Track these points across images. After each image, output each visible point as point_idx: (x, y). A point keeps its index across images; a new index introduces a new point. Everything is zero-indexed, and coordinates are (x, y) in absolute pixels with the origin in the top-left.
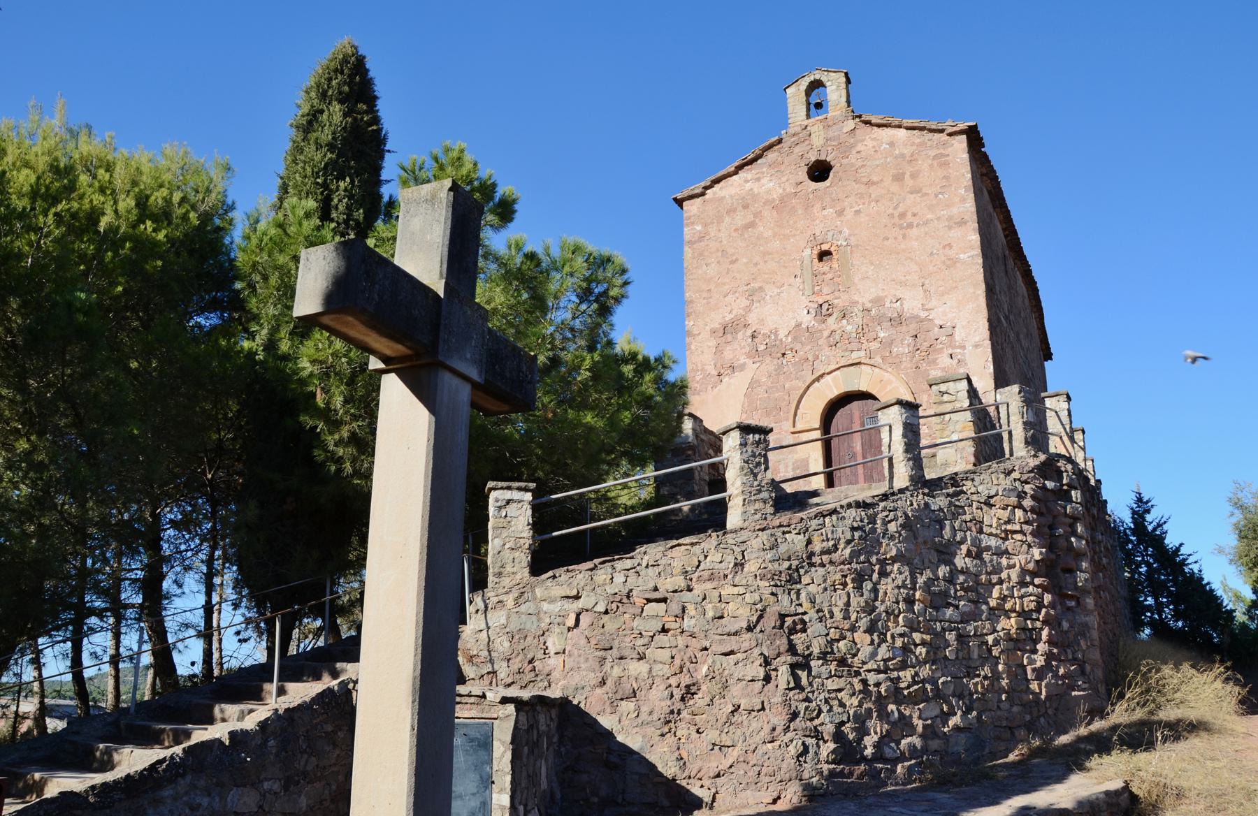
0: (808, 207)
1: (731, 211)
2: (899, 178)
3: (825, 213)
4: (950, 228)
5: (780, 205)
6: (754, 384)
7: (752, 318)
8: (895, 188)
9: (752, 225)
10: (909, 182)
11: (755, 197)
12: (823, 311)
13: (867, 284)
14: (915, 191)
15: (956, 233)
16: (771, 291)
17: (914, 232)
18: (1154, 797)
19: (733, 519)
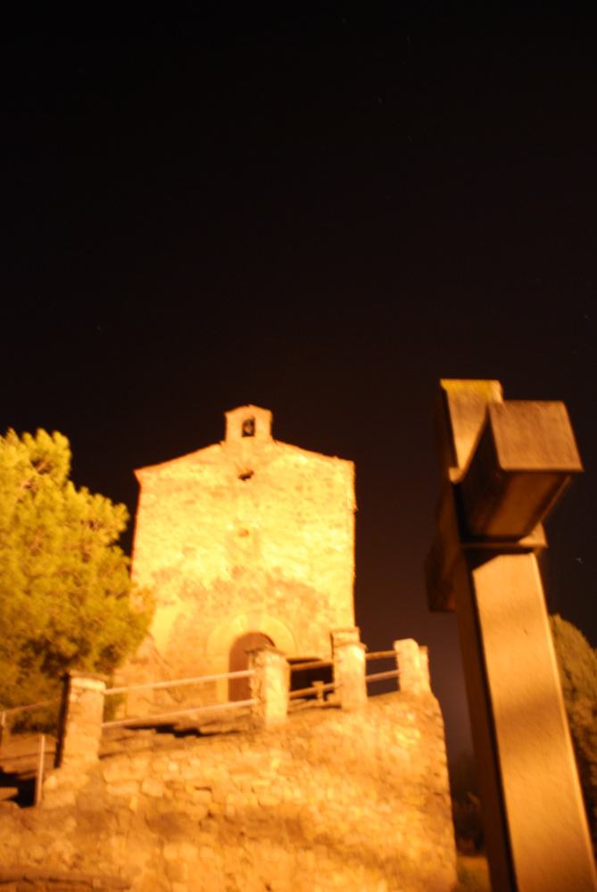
0: (235, 496)
1: (179, 490)
2: (299, 488)
3: (243, 510)
4: (331, 527)
5: (217, 493)
6: (181, 616)
7: (185, 568)
8: (296, 494)
9: (191, 502)
10: (306, 493)
11: (197, 483)
12: (236, 572)
13: (273, 557)
14: (310, 499)
15: (335, 532)
16: (201, 551)
17: (307, 527)
18: (425, 790)
19: (258, 435)
